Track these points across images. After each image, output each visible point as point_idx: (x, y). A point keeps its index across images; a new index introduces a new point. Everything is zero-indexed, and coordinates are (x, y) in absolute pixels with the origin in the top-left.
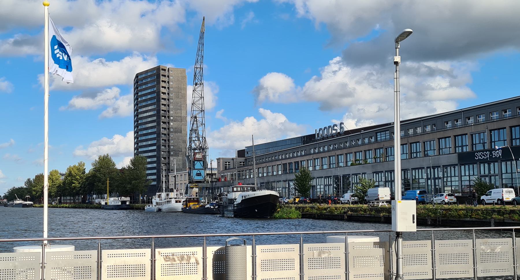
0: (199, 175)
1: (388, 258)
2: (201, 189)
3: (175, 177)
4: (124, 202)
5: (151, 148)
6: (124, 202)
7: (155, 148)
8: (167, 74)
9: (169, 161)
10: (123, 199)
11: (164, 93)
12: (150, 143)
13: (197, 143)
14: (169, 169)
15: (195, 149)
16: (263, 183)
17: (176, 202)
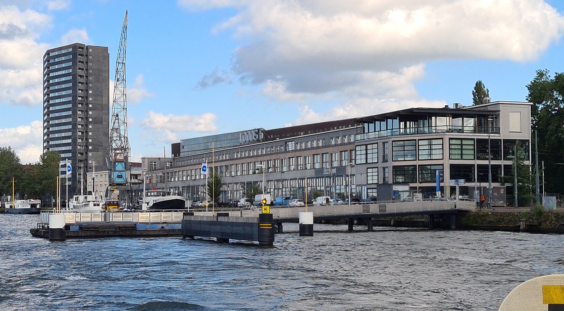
0: (120, 177)
1: (151, 233)
2: (122, 192)
3: (93, 179)
4: (33, 206)
5: (64, 141)
6: (33, 206)
7: (70, 141)
9: (87, 157)
10: (33, 201)
11: (81, 76)
12: (63, 135)
13: (118, 142)
14: (87, 167)
15: (115, 150)
16: (184, 187)
17: (95, 205)
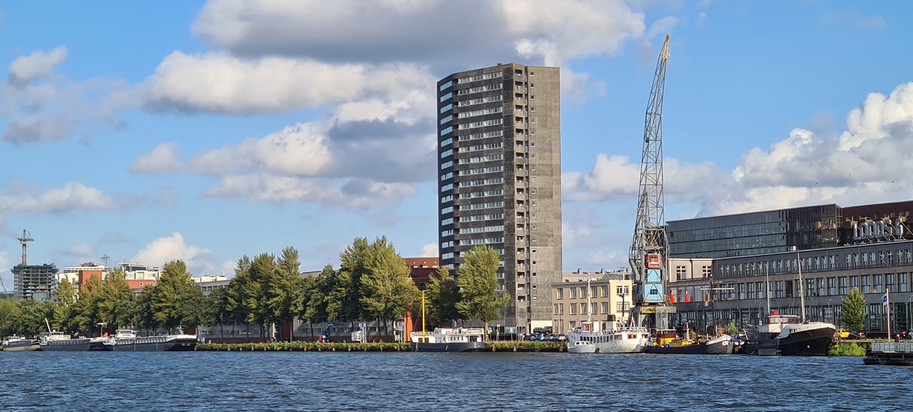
4: (473, 338)
8: (523, 80)
11: (518, 119)
17: (630, 337)
